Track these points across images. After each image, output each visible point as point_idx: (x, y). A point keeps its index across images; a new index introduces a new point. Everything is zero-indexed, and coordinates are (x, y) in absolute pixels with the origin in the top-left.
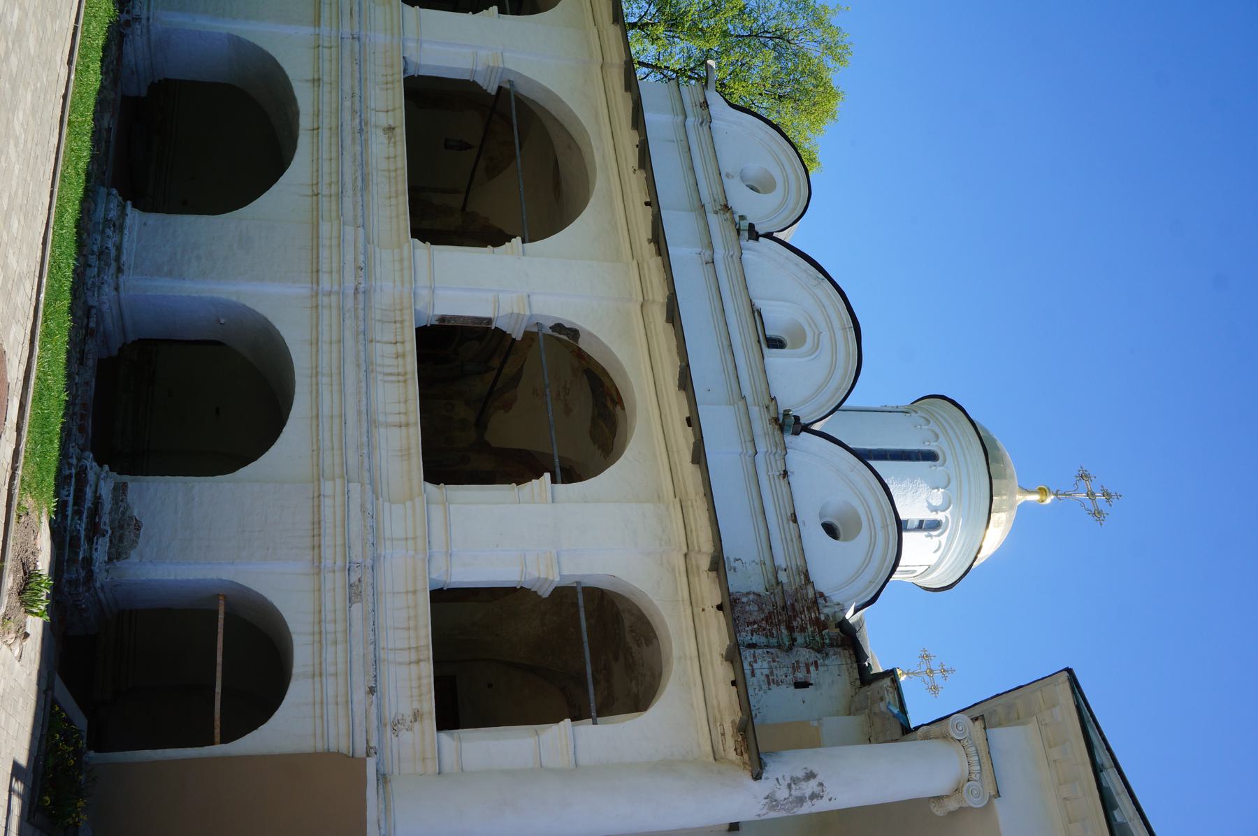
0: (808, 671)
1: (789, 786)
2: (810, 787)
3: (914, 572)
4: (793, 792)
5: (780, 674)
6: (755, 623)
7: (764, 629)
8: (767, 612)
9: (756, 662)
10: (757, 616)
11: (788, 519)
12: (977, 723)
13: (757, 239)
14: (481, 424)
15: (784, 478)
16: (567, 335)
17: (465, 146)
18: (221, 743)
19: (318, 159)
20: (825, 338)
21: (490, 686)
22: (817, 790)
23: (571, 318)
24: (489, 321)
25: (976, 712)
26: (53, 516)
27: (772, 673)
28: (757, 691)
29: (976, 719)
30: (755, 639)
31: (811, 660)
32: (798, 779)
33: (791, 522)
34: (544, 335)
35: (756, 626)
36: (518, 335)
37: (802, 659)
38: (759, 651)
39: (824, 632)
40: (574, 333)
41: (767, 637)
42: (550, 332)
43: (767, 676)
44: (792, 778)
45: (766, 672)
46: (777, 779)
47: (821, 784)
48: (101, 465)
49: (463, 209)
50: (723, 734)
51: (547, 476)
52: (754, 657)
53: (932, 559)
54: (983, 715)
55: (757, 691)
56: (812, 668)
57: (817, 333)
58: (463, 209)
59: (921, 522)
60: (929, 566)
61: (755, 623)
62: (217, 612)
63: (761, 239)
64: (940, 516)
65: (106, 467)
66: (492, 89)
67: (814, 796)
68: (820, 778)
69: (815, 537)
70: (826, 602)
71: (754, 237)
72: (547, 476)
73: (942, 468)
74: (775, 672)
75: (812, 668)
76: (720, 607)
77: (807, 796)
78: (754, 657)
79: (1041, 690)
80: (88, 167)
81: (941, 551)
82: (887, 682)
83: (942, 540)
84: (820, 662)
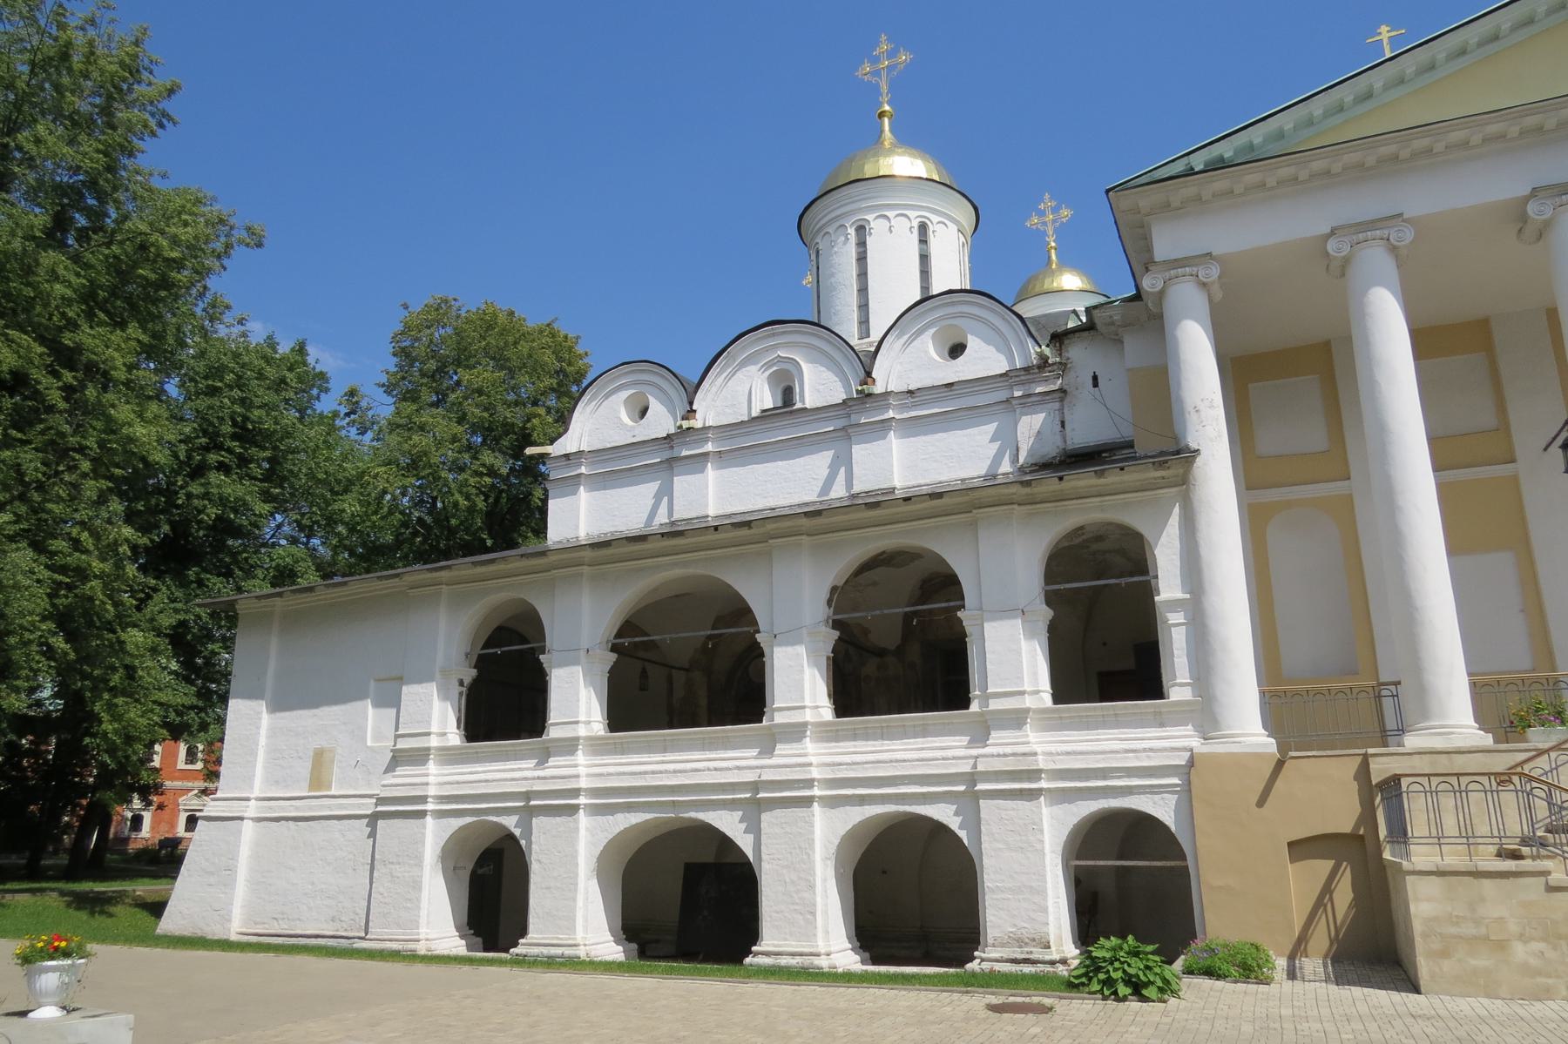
3: (963, 243)
11: (951, 391)
12: (1150, 268)
13: (695, 411)
14: (881, 653)
15: (913, 393)
16: (834, 595)
17: (644, 671)
18: (1186, 860)
23: (824, 594)
24: (828, 658)
25: (1138, 269)
26: (64, 394)
29: (1147, 268)
33: (953, 388)
34: (834, 614)
36: (836, 634)
40: (834, 589)
42: (832, 609)
48: (974, 958)
49: (687, 670)
50: (1163, 478)
51: (959, 614)
53: (953, 228)
54: (1145, 264)
57: (779, 359)
58: (687, 670)
59: (920, 241)
60: (959, 230)
62: (1118, 867)
63: (694, 408)
64: (915, 224)
65: (976, 953)
66: (613, 657)
69: (963, 369)
71: (693, 414)
73: (872, 223)
76: (1061, 479)
81: (946, 221)
82: (1096, 313)
83: (937, 221)
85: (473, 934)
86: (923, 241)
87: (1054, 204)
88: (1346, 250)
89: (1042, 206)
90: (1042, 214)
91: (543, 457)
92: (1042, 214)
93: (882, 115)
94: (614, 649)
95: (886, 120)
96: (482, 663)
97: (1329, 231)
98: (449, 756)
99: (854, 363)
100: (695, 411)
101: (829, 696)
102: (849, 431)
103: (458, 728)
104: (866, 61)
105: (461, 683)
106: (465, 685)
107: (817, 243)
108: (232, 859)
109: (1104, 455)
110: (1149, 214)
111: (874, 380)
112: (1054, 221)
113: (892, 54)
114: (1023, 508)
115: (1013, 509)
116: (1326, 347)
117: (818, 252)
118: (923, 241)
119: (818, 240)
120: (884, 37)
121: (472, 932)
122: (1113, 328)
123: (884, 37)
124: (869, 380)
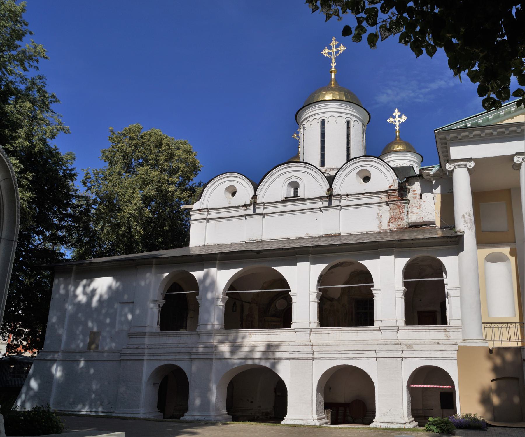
0: (416, 194)
1: (467, 223)
2: (466, 216)
4: (468, 222)
5: (417, 204)
6: (400, 211)
7: (402, 208)
8: (396, 207)
9: (413, 212)
10: (398, 210)
13: (257, 196)
19: (159, 335)
20: (295, 174)
21: (421, 300)
22: (468, 214)
27: (417, 207)
28: (423, 212)
30: (405, 211)
31: (413, 192)
32: (464, 220)
35: (401, 211)
37: (412, 196)
38: (409, 211)
39: (404, 188)
41: (405, 207)
43: (418, 208)
44: (464, 222)
45: (416, 208)
46: (465, 227)
47: (466, 213)
52: (411, 212)
55: (423, 212)
56: (415, 192)
60: (363, 124)
61: (400, 211)
67: (469, 216)
68: (465, 214)
69: (368, 187)
70: (393, 185)
72: (372, 289)
74: (416, 206)
75: (415, 192)
77: (469, 218)
78: (411, 212)
79: (264, 206)
80: (196, 421)
84: (413, 190)
85: (159, 412)
86: (348, 128)
87: (399, 113)
88: (521, 161)
89: (394, 114)
90: (394, 117)
91: (190, 209)
92: (394, 117)
93: (332, 72)
94: (227, 295)
95: (333, 74)
96: (166, 297)
97: (515, 153)
98: (153, 335)
99: (325, 181)
100: (257, 196)
101: (318, 318)
102: (322, 209)
103: (158, 325)
104: (326, 47)
105: (159, 306)
106: (161, 307)
107: (304, 124)
108: (50, 378)
109: (423, 226)
110: (448, 141)
111: (333, 189)
112: (399, 121)
113: (337, 46)
114: (397, 249)
115: (394, 249)
116: (509, 190)
117: (304, 128)
118: (348, 128)
119: (304, 123)
120: (334, 39)
121: (159, 410)
122: (429, 177)
123: (334, 39)
124: (331, 189)
